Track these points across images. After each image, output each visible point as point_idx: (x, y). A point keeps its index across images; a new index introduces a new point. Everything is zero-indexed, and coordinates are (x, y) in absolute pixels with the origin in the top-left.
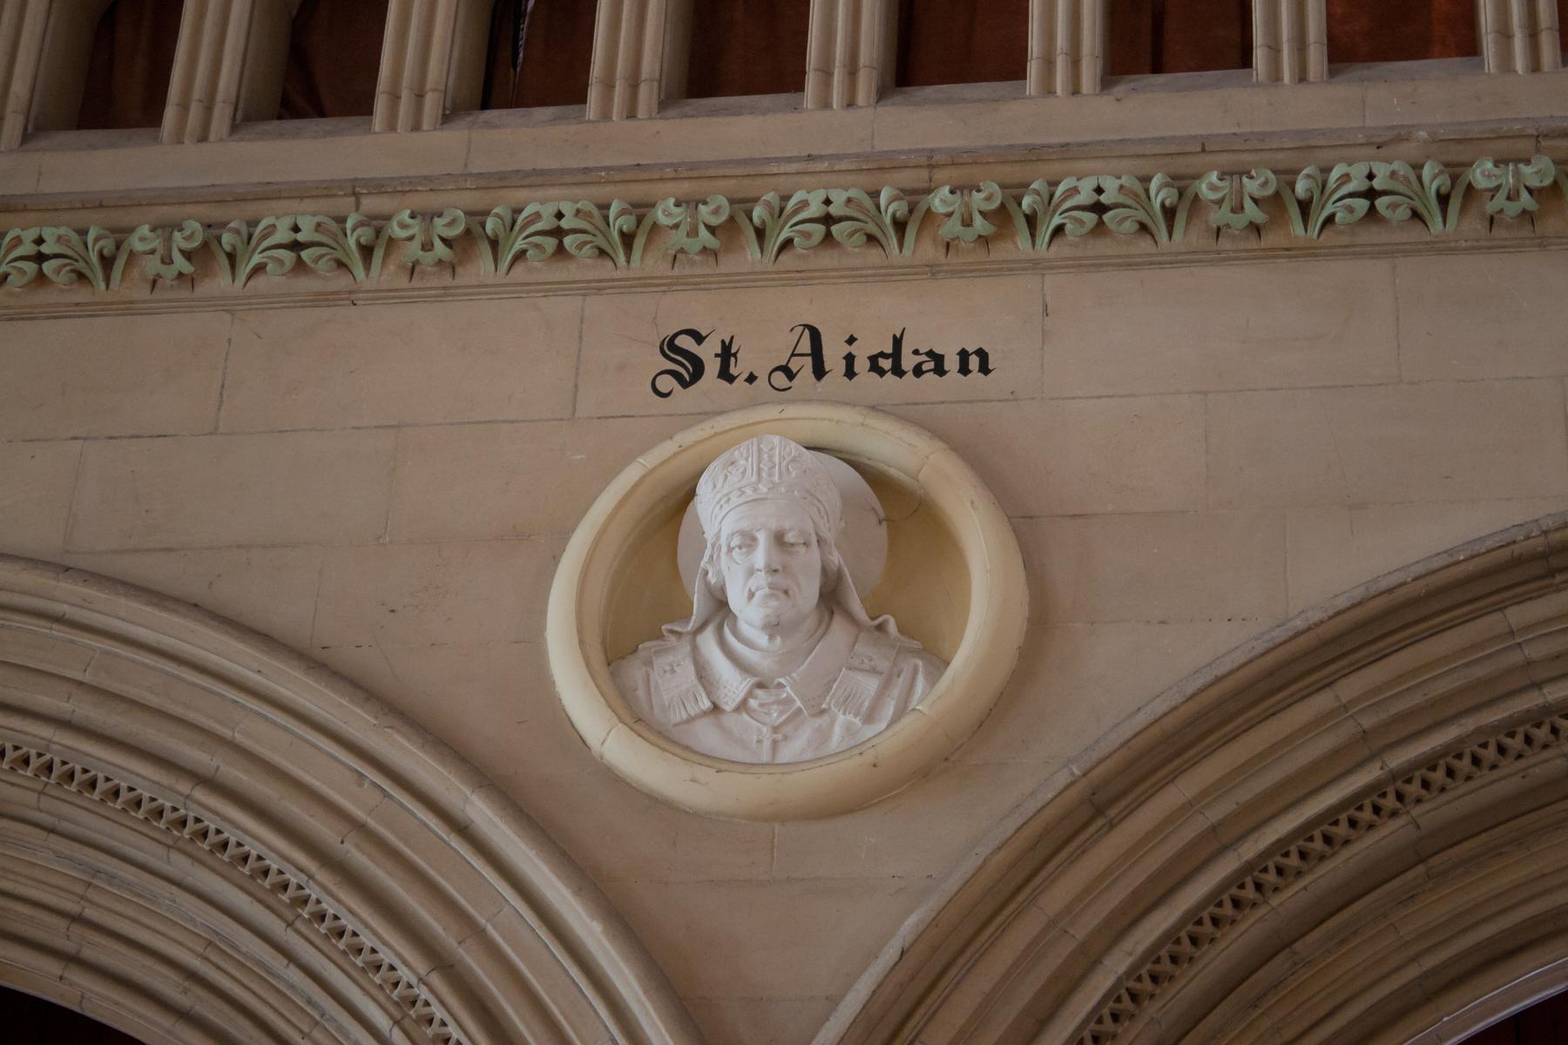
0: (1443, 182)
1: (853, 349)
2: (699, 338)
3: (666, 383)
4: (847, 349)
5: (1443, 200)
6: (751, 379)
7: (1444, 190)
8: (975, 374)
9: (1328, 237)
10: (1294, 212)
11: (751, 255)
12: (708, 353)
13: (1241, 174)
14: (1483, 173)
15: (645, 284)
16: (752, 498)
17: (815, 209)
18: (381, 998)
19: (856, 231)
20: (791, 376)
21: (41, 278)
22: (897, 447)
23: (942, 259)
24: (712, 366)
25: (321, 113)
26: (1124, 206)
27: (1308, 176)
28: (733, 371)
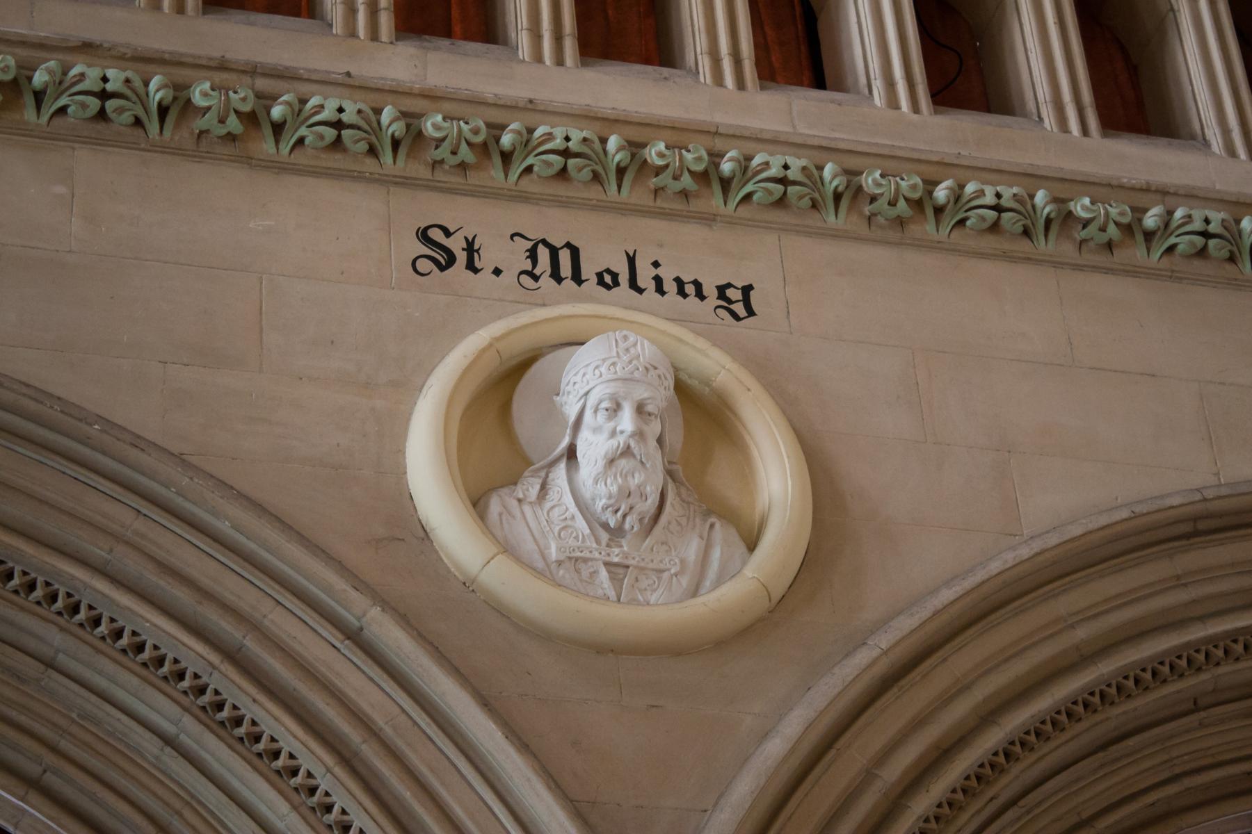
0: (398, 128)
1: (660, 272)
2: (448, 234)
3: (424, 265)
4: (654, 272)
5: (396, 144)
6: (497, 272)
7: (165, 103)
8: (693, 300)
9: (744, 211)
10: (29, 100)
11: (715, 201)
12: (456, 245)
13: (681, 148)
14: (434, 125)
15: (404, 182)
16: (600, 384)
17: (91, 83)
18: (245, 752)
19: (585, 166)
20: (536, 278)
21: (337, 144)
22: (714, 364)
23: (651, 204)
24: (461, 257)
25: (448, 34)
26: (359, 128)
27: (287, 103)
28: (478, 264)
